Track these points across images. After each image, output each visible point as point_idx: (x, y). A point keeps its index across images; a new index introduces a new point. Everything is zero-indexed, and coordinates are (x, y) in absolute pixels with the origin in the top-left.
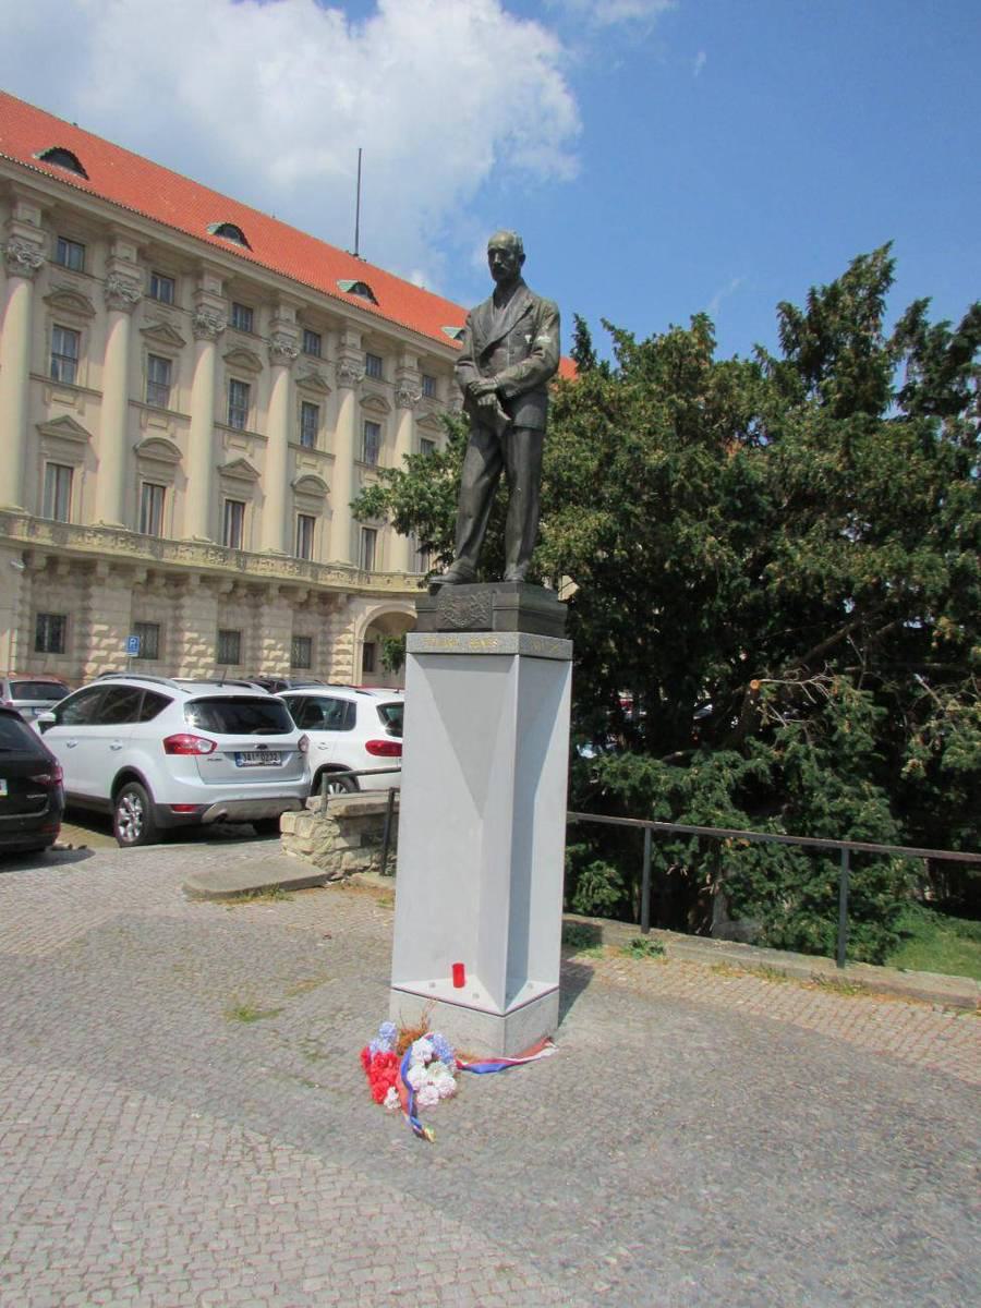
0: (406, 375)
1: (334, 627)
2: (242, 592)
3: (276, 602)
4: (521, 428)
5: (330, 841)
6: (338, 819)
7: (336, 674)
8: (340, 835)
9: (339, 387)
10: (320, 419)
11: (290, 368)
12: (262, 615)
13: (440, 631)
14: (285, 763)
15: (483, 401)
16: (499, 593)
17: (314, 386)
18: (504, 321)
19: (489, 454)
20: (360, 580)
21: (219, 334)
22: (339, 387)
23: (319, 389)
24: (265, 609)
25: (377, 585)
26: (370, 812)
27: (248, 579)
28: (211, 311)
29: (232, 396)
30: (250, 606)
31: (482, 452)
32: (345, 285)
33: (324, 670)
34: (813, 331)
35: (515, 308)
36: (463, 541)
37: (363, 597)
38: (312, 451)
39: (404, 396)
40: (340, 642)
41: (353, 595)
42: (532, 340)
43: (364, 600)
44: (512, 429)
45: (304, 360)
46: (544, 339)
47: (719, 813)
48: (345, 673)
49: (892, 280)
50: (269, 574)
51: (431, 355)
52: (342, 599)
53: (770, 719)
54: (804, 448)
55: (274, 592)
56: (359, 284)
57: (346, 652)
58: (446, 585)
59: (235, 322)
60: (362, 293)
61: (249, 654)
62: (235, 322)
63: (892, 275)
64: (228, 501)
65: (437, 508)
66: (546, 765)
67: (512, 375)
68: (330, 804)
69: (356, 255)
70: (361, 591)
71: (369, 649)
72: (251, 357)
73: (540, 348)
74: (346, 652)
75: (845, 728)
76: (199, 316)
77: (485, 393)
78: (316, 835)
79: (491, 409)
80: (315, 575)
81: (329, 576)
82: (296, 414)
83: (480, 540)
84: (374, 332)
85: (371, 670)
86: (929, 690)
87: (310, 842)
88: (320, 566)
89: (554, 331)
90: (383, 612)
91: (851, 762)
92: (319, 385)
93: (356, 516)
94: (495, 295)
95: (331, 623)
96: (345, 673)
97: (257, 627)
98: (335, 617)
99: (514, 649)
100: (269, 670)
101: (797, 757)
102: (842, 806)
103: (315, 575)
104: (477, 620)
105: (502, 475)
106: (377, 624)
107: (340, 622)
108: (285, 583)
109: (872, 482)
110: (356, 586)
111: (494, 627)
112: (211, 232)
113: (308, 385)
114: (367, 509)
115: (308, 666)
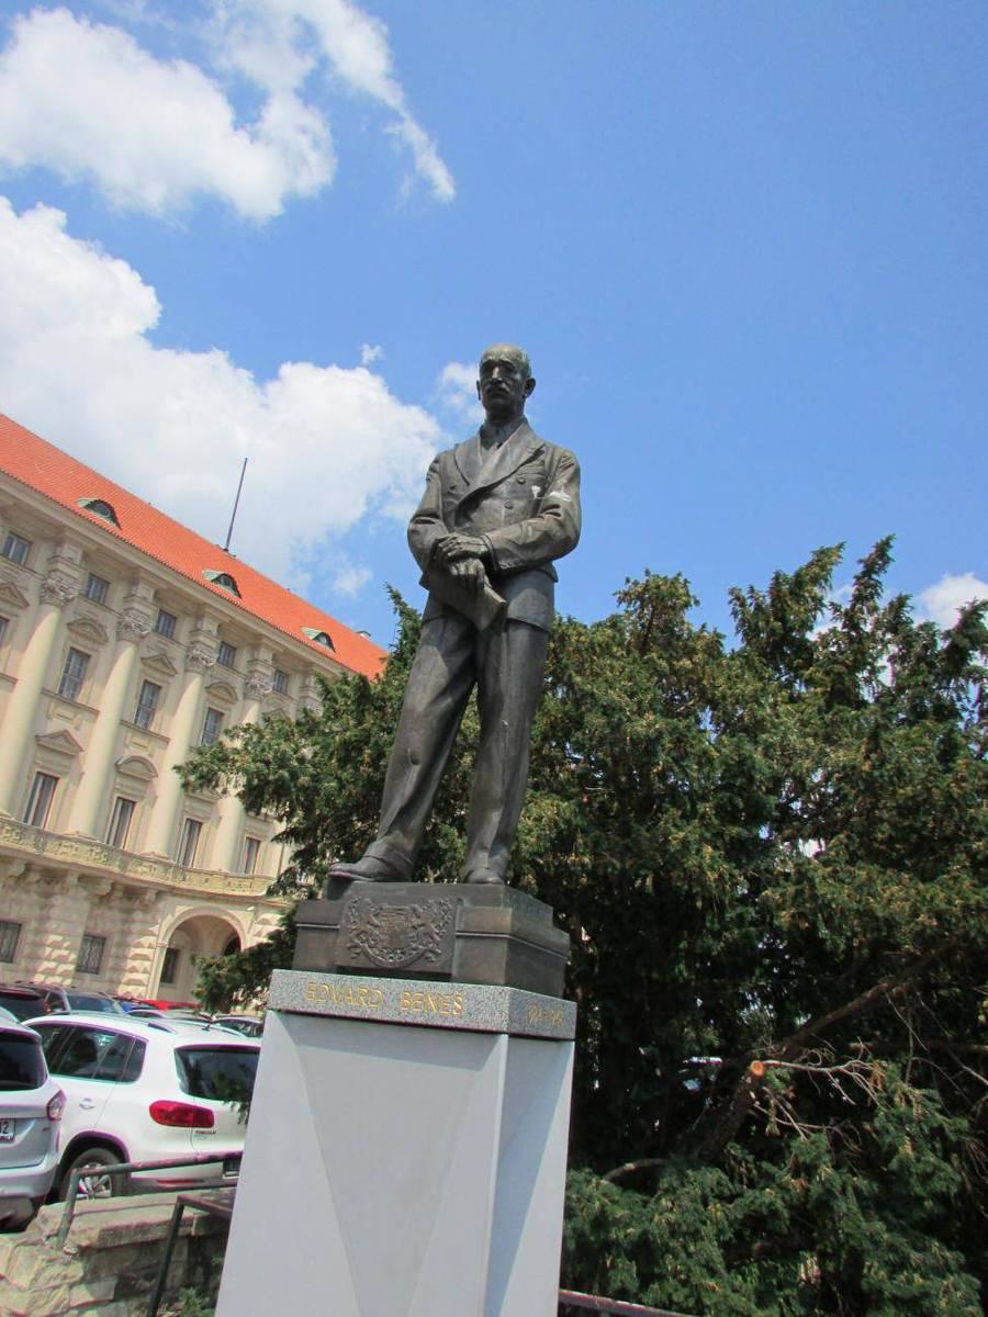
0: (259, 668)
1: (136, 927)
2: (34, 877)
3: (72, 892)
4: (517, 623)
5: (61, 1293)
6: (84, 1252)
7: (129, 983)
8: (83, 1280)
9: (186, 671)
10: (160, 701)
11: (137, 645)
12: (53, 906)
13: (342, 970)
14: (20, 1138)
15: (461, 569)
16: (466, 904)
17: (159, 666)
18: (489, 466)
19: (459, 659)
20: (175, 877)
21: (68, 601)
22: (186, 671)
23: (165, 669)
24: (58, 900)
25: (193, 883)
26: (139, 1238)
27: (45, 863)
28: (65, 578)
29: (68, 666)
30: (40, 894)
31: (446, 655)
32: (210, 575)
33: (120, 952)
34: (776, 619)
35: (517, 451)
36: (398, 803)
37: (175, 895)
38: (145, 732)
39: (254, 687)
40: (139, 945)
41: (163, 892)
42: (541, 494)
43: (176, 899)
44: (502, 621)
45: (155, 638)
46: (558, 495)
47: (712, 1283)
48: (139, 983)
49: (889, 559)
50: (70, 859)
51: (287, 652)
52: (150, 896)
53: (779, 1125)
54: (810, 740)
55: (72, 879)
56: (224, 575)
57: (145, 958)
58: (361, 882)
59: (88, 593)
60: (226, 584)
61: (27, 950)
62: (88, 593)
63: (890, 553)
64: (39, 773)
65: (304, 780)
66: (519, 1255)
67: (512, 536)
68: (76, 1225)
69: (226, 550)
70: (174, 888)
71: (172, 956)
72: (98, 629)
73: (557, 506)
74: (145, 958)
75: (907, 1149)
76: (50, 581)
77: (466, 556)
78: (41, 1280)
79: (470, 585)
80: (124, 866)
81: (139, 869)
82: (136, 689)
83: (430, 794)
84: (233, 622)
85: (171, 981)
86: (949, 1079)
87: (27, 1296)
88: (131, 856)
89: (573, 490)
90: (194, 915)
91: (922, 1207)
92: (165, 665)
93: (186, 785)
94: (483, 432)
95: (133, 921)
96: (139, 983)
97: (44, 919)
98: (138, 915)
99: (499, 1021)
100: (50, 972)
101: (829, 1192)
102: (915, 1290)
103: (124, 866)
104: (421, 956)
105: (475, 690)
106: (186, 928)
107: (143, 922)
108: (87, 872)
109: (909, 788)
110: (169, 883)
111: (454, 972)
112: (82, 504)
113: (153, 664)
114: (201, 777)
115: (97, 971)
